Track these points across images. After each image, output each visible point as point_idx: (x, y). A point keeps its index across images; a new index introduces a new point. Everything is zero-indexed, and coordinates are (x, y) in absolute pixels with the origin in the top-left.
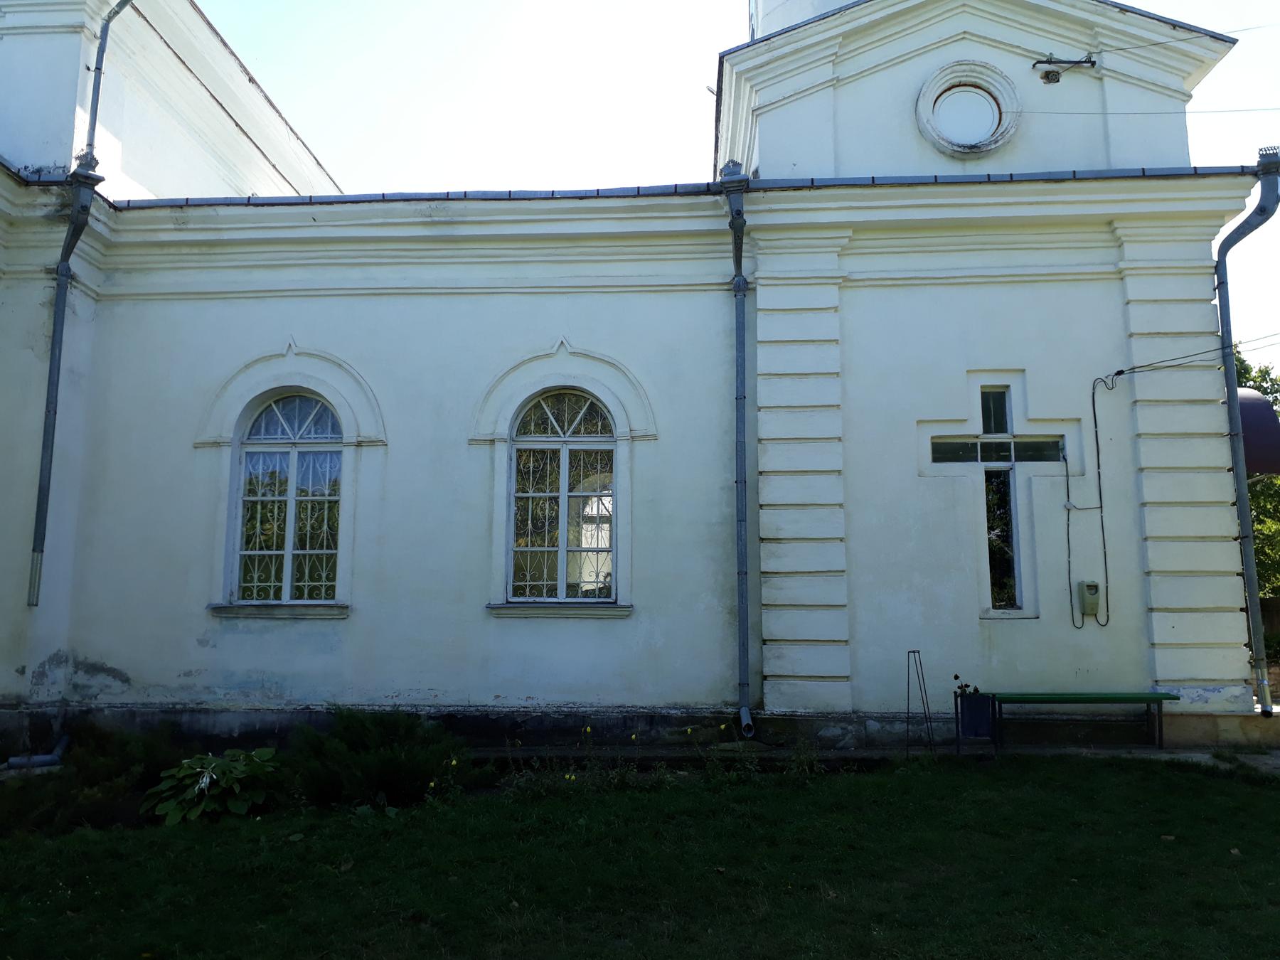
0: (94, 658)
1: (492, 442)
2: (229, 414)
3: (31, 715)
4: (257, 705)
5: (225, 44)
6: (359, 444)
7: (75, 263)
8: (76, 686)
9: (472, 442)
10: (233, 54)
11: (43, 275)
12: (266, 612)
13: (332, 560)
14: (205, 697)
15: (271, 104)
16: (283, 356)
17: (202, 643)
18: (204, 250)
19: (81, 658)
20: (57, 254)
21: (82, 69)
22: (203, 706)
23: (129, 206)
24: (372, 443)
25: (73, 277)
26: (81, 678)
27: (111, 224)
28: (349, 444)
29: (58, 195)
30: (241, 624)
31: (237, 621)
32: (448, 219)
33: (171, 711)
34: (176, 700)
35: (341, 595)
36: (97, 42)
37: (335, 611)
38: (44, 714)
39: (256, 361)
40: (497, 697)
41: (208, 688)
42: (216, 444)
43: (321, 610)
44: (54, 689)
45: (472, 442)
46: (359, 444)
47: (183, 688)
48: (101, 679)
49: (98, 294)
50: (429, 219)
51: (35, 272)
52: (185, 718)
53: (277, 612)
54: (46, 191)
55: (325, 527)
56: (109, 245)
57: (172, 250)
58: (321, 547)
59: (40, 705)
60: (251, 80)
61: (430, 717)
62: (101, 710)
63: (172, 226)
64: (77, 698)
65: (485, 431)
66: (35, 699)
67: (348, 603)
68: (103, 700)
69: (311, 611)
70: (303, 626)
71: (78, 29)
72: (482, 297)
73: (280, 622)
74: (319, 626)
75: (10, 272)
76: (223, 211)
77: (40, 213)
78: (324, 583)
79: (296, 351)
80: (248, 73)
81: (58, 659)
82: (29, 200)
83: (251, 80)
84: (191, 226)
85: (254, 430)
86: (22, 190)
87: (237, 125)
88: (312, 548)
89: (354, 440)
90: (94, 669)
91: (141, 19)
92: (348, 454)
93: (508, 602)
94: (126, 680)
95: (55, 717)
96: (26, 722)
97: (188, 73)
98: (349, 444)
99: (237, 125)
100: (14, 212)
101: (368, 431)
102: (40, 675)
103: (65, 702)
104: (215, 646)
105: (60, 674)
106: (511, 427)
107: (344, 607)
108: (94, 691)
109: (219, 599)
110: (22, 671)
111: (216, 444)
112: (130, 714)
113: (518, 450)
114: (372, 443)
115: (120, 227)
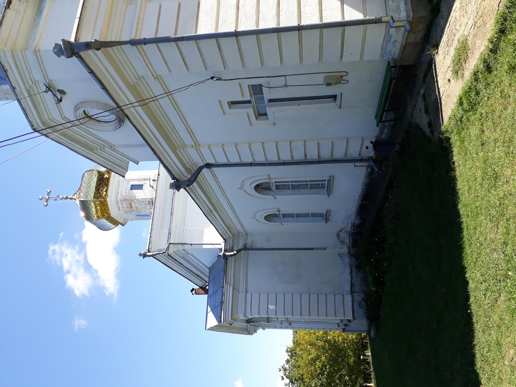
38: (352, 242)
56: (233, 235)
59: (350, 242)
66: (348, 243)
71: (184, 250)
81: (338, 236)
95: (353, 238)
96: (354, 249)
101: (266, 177)
102: (342, 242)
106: (269, 195)
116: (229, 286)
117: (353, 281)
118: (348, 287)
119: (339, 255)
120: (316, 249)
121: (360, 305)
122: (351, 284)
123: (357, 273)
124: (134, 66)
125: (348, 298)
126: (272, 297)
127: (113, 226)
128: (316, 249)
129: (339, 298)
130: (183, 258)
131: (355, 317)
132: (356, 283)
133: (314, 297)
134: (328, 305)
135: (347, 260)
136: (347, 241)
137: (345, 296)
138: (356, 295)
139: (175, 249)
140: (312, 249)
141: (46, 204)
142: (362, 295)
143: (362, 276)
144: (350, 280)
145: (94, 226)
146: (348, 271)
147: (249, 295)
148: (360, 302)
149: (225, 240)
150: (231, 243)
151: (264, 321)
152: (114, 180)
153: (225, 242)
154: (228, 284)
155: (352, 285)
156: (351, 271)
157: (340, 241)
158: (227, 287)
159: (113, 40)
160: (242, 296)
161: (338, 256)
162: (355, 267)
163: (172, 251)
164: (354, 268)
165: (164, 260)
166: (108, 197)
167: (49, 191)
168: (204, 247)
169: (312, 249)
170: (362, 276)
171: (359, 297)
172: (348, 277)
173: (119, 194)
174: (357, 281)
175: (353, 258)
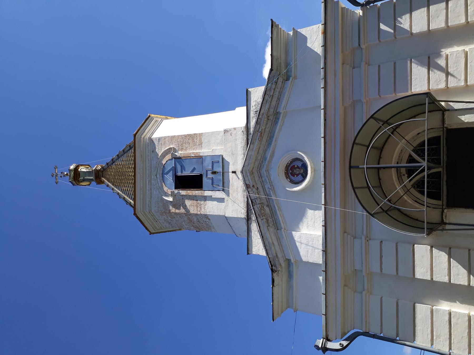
159: (311, 261)
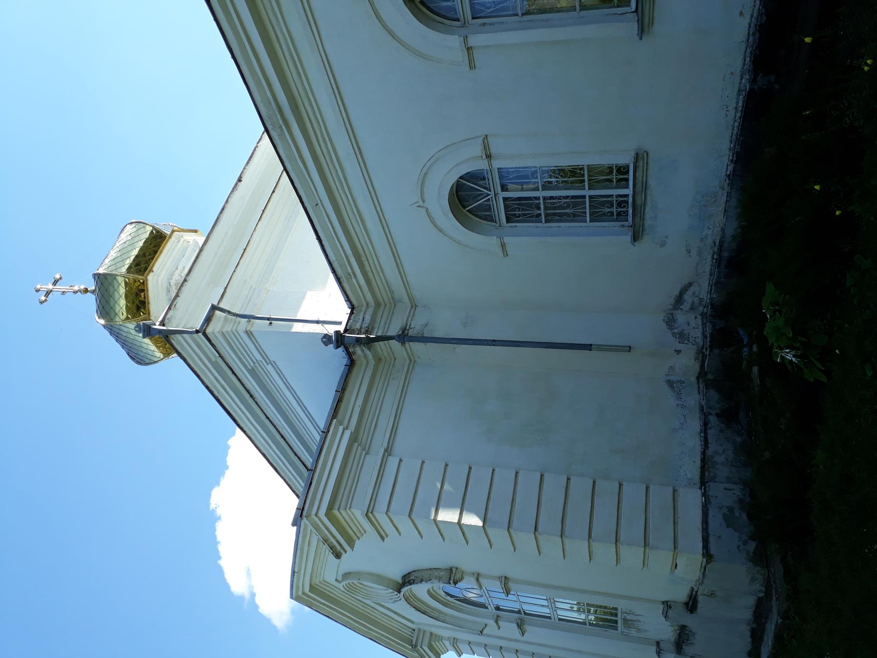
0: (672, 301)
1: (469, 49)
2: (481, 242)
3: (712, 347)
4: (721, 208)
5: (223, 209)
6: (489, 157)
7: (394, 331)
8: (692, 308)
9: (472, 66)
10: (227, 201)
11: (407, 345)
12: (639, 211)
13: (591, 168)
14: (710, 241)
15: (251, 157)
16: (427, 209)
17: (663, 244)
18: (364, 258)
19: (671, 307)
20: (393, 342)
21: (271, 329)
22: (717, 244)
23: (348, 299)
24: (486, 147)
25: (404, 330)
26: (686, 306)
27: (364, 309)
28: (490, 165)
29: (354, 346)
30: (648, 222)
31: (646, 224)
32: (277, 113)
33: (718, 262)
34: (710, 257)
35: (626, 159)
36: (253, 320)
37: (640, 163)
38: (711, 335)
39: (435, 226)
40: (741, 14)
41: (702, 239)
42: (503, 246)
43: (639, 174)
44: (693, 324)
45: (472, 66)
46: (489, 157)
47: (700, 254)
48: (688, 297)
49: (412, 307)
50: (284, 127)
51: (406, 350)
52: (725, 254)
53: (639, 202)
54: (354, 353)
55: (567, 211)
56: (378, 305)
57: (370, 274)
58: (585, 213)
59: (704, 336)
60: (240, 180)
61: (753, 81)
62: (712, 299)
63: (354, 280)
64: (701, 308)
65: (461, 56)
66: (700, 341)
67: (633, 154)
68: (704, 295)
69: (639, 181)
70: (652, 182)
71: (249, 334)
72: (334, 69)
73: (648, 198)
74: (652, 170)
75: (409, 357)
76: (332, 258)
77: (368, 352)
78: (614, 209)
79: (421, 203)
80: (236, 184)
81: (670, 321)
82: (362, 358)
83: (240, 180)
84: (350, 270)
85: (490, 219)
86: (357, 362)
87: (273, 192)
88: (583, 175)
89: (486, 161)
90: (679, 300)
91: (228, 290)
92: (497, 164)
93: (636, 11)
94: (690, 284)
95: (714, 325)
96: (716, 351)
97: (251, 243)
98: (490, 165)
99: (273, 192)
100: (372, 363)
101: (478, 150)
102: (682, 337)
103: (703, 315)
104: (667, 237)
105: (681, 318)
106: (448, 31)
107: (637, 157)
108: (696, 300)
109: (628, 238)
110: (678, 352)
111: (503, 246)
112: (717, 285)
113: (473, 18)
114: (486, 147)
115: (364, 303)
116: (341, 428)
117: (709, 452)
118: (692, 468)
119: (670, 383)
120: (601, 348)
121: (729, 520)
122: (703, 460)
123: (721, 431)
124: (422, 477)
125: (692, 501)
126: (458, 473)
127: (159, 354)
128: (601, 348)
129: (661, 496)
130: (253, 372)
131: (713, 551)
132: (720, 459)
133: (581, 487)
134: (623, 511)
135: (693, 399)
136: (698, 333)
137: (682, 492)
138: (717, 489)
139: (228, 328)
140: (588, 347)
141: (43, 298)
142: (738, 490)
143: (739, 439)
144: (699, 449)
145: (118, 346)
146: (696, 425)
147: (393, 462)
148: (731, 509)
149: (352, 308)
150: (368, 318)
151: (440, 579)
152: (176, 245)
153: (352, 313)
154: (341, 423)
155: (705, 462)
156: (706, 424)
157: (673, 334)
158: (336, 429)
160: (372, 462)
161: (666, 387)
162: (718, 415)
163: (217, 330)
164: (713, 419)
165: (210, 380)
166: (151, 274)
167: (58, 276)
168: (298, 328)
169: (588, 347)
170: (739, 439)
171: (727, 494)
172: (694, 443)
173: (177, 272)
174: (723, 451)
175: (713, 393)
